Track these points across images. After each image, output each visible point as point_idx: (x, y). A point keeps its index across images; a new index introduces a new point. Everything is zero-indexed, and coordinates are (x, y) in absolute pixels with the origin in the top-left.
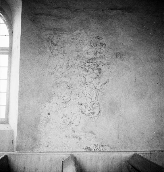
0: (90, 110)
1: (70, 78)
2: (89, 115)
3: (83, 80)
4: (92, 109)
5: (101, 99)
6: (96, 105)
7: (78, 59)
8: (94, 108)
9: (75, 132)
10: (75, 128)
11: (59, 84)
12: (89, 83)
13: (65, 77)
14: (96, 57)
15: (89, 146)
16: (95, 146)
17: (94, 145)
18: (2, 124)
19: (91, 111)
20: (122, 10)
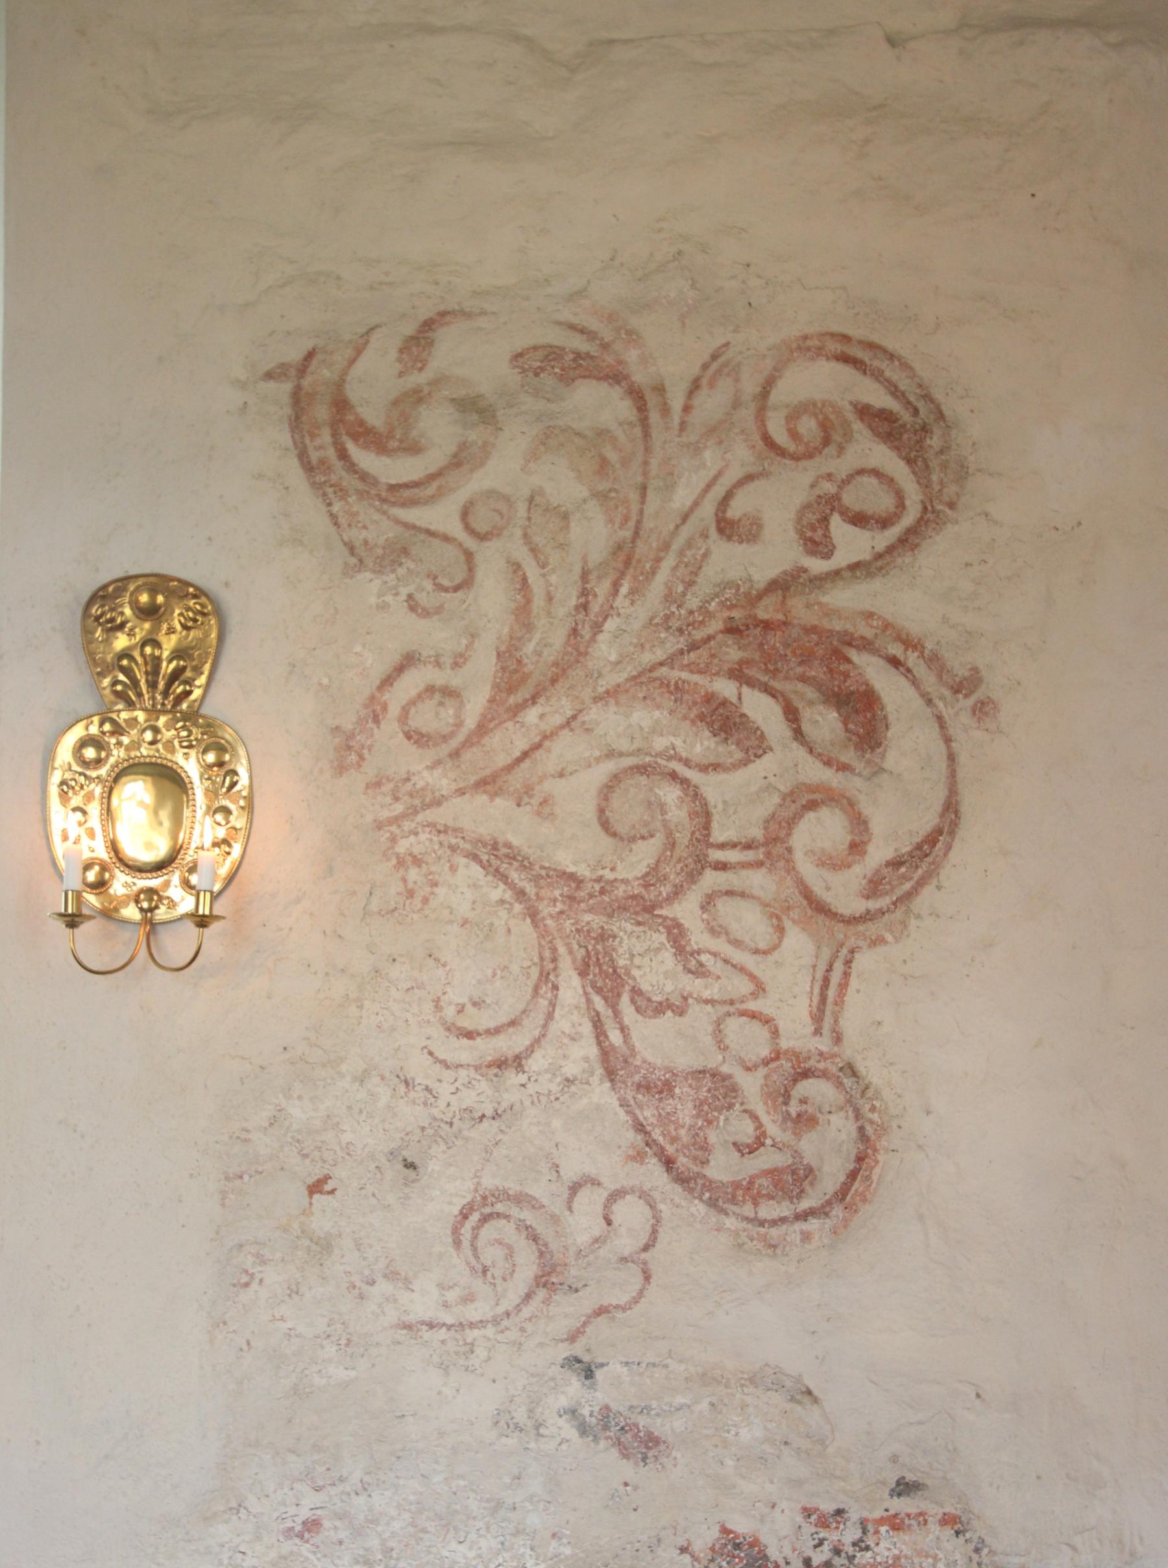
0: (759, 1142)
1: (535, 801)
2: (747, 1191)
3: (678, 813)
4: (773, 1129)
5: (191, 1175)
6: (816, 1090)
7: (624, 590)
8: (804, 1121)
9: (599, 1374)
10: (602, 1328)
11: (417, 861)
12: (749, 856)
13: (488, 784)
14: (817, 566)
15: (742, 1526)
16: (808, 1529)
17: (807, 1512)
18: (432, 528)
19: (767, 1159)
20: (1113, 37)
